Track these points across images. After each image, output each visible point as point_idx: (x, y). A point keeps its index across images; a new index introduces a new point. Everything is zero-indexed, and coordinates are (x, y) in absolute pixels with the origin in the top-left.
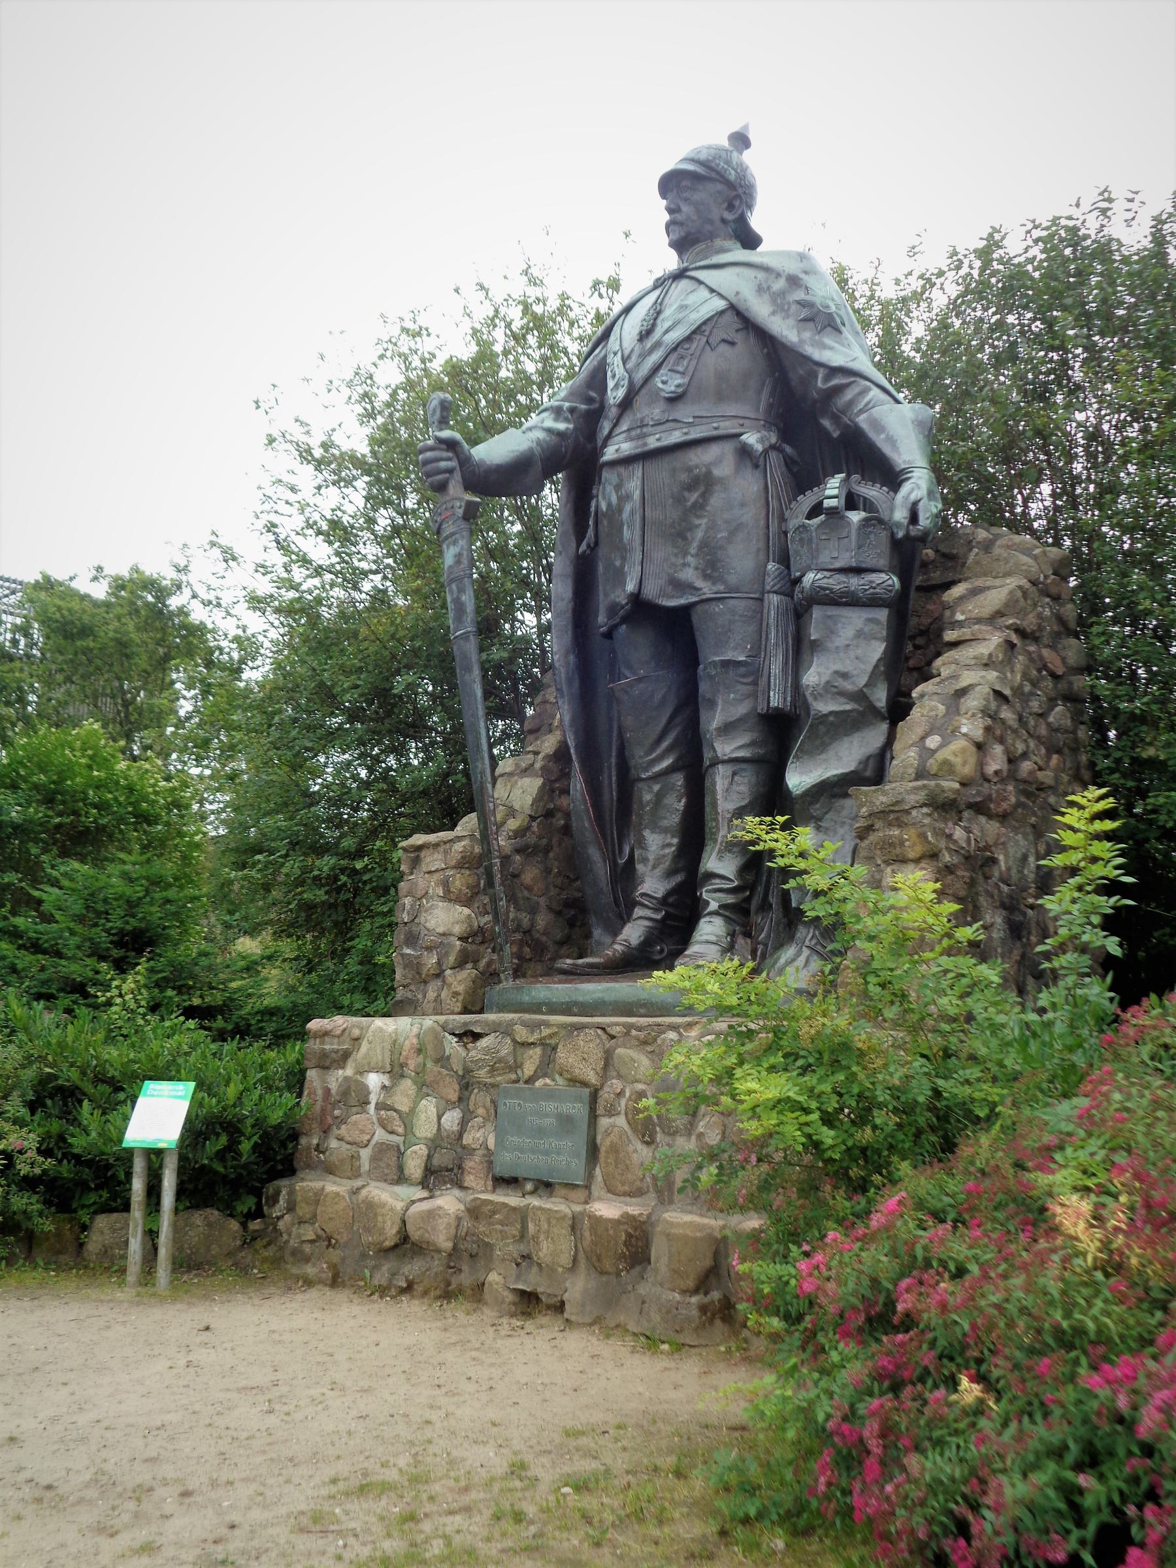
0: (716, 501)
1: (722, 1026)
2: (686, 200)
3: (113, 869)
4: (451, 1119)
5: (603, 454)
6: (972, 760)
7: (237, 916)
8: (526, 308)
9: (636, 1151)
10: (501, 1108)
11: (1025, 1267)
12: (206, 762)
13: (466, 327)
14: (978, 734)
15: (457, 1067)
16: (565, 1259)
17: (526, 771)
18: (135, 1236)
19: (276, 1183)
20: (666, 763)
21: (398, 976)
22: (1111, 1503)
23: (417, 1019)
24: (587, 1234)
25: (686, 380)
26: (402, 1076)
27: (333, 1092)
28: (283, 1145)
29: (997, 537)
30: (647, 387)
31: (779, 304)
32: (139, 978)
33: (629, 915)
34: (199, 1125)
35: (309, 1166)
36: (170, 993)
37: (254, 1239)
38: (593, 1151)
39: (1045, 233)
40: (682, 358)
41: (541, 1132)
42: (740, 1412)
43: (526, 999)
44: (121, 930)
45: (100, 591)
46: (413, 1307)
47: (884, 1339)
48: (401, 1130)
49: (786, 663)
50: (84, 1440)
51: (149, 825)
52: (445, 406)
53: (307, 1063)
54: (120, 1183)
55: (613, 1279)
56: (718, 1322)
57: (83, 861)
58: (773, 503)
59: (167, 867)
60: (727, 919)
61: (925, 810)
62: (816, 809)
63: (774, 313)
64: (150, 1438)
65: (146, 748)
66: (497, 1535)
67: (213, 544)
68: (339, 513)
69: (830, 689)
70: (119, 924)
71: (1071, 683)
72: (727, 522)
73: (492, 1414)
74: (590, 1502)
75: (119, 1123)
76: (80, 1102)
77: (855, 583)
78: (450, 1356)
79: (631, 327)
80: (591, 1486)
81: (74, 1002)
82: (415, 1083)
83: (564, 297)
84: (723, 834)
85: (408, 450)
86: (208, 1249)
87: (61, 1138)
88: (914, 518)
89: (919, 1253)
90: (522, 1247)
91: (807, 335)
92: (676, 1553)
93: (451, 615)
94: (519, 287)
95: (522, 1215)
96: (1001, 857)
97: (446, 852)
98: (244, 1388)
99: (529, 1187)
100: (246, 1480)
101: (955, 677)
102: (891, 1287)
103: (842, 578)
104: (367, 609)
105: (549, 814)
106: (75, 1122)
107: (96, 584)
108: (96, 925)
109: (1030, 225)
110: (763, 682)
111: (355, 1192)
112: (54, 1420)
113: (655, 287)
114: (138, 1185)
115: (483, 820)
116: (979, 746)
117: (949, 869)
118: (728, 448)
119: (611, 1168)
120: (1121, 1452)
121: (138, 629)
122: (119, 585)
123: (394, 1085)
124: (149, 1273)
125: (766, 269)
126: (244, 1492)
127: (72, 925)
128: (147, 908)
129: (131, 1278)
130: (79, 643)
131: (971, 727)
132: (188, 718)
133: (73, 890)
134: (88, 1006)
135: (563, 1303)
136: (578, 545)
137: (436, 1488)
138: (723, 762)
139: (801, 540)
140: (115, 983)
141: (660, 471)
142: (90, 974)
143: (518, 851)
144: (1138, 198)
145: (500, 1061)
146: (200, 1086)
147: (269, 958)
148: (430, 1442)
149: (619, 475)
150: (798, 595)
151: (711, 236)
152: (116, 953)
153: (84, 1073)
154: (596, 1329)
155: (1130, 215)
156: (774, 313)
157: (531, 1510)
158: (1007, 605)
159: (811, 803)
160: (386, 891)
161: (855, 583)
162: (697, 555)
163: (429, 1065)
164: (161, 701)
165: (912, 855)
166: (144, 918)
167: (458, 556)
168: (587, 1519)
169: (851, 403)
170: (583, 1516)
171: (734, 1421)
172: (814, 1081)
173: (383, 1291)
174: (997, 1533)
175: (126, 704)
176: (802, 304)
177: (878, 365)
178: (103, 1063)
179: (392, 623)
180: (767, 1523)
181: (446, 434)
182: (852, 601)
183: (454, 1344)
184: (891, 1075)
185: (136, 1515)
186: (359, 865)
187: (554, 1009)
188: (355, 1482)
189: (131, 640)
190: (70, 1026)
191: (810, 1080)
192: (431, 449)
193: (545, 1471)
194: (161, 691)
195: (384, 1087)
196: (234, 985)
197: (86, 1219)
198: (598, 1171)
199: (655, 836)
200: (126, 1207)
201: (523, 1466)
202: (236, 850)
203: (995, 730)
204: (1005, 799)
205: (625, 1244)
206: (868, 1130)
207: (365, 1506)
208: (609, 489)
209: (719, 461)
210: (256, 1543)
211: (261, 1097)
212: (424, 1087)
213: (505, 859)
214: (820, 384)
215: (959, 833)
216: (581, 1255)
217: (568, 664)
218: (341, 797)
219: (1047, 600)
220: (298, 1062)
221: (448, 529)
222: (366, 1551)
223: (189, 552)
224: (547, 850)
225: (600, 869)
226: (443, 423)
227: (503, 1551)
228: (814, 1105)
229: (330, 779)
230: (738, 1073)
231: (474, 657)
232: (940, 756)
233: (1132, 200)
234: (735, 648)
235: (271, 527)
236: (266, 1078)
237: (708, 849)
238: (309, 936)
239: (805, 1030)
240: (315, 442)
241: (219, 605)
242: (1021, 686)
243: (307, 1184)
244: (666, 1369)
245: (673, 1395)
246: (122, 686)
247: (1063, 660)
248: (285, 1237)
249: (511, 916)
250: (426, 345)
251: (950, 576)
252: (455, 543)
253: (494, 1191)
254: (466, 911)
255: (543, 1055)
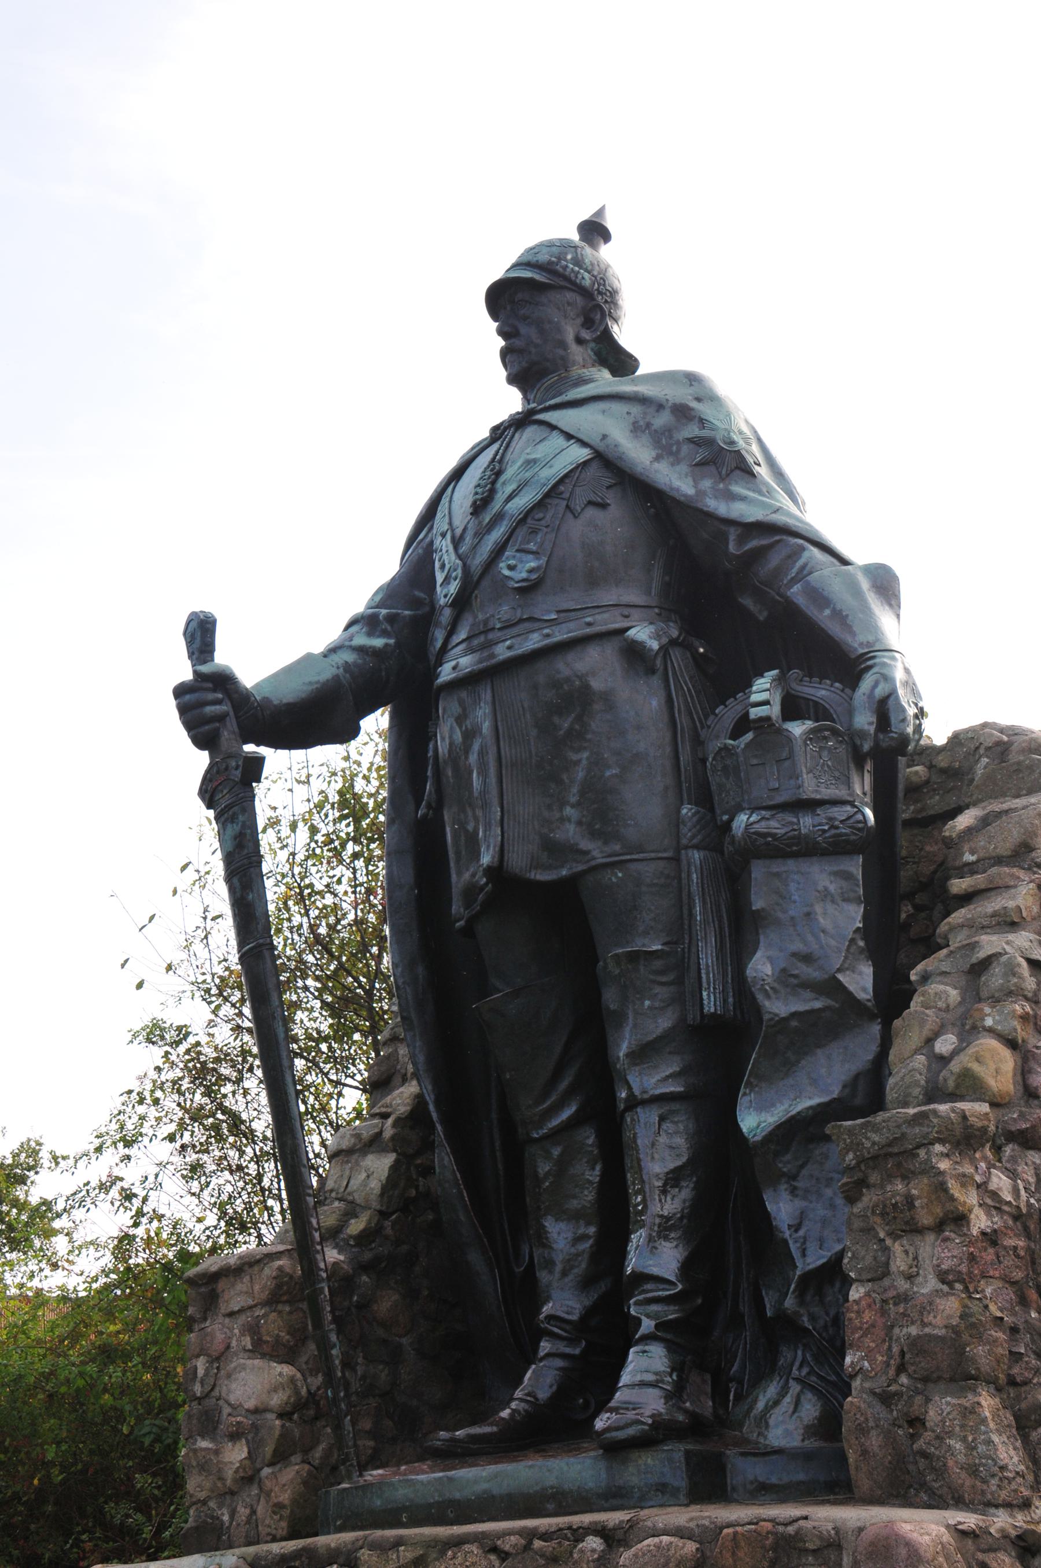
2: (525, 318)
5: (438, 676)
20: (566, 1114)
25: (543, 561)
60: (671, 1347)
62: (786, 1163)
63: (658, 458)
91: (706, 484)
125: (642, 400)
139: (725, 768)
143: (365, 1267)
149: (461, 703)
150: (728, 848)
156: (658, 458)
176: (696, 442)
199: (562, 1225)
214: (732, 548)
232: (955, 1066)
234: (646, 933)
251: (953, 801)
254: (287, 1370)
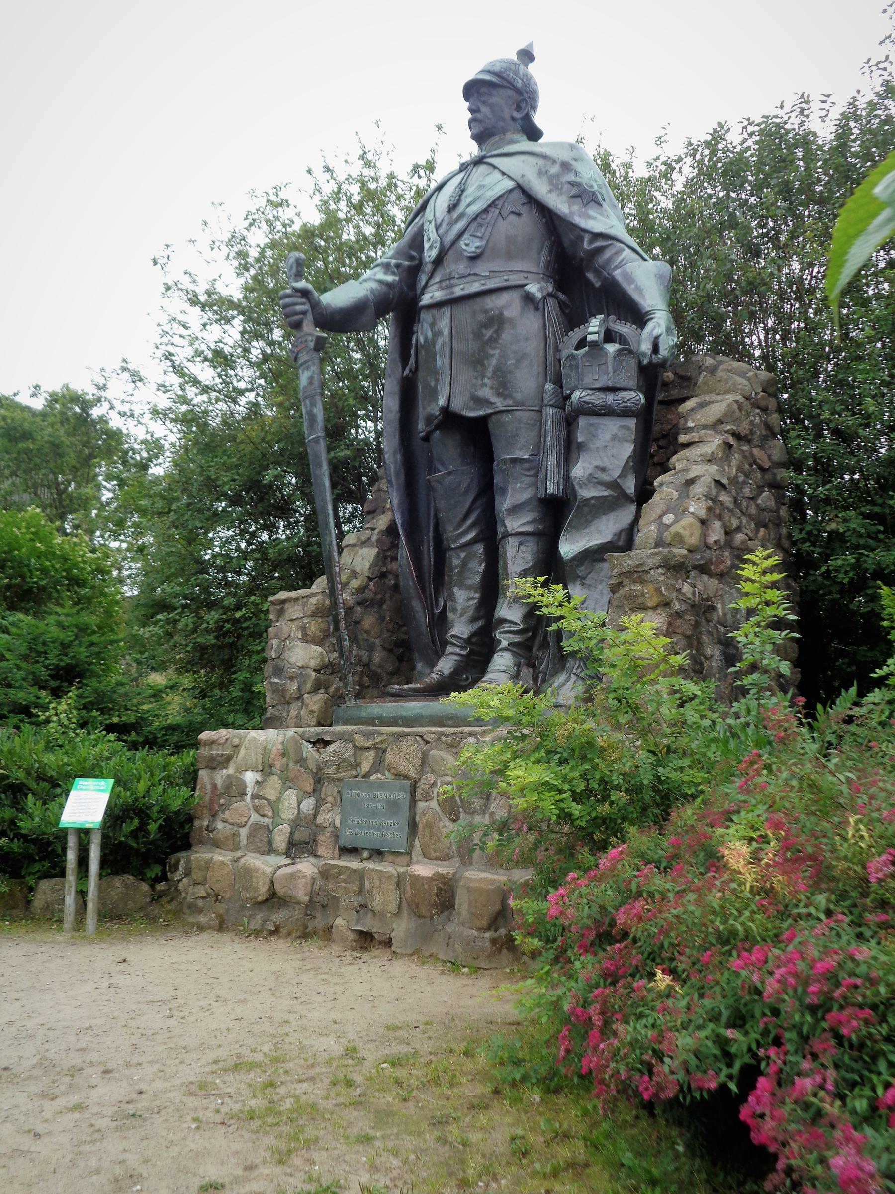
0: (506, 336)
1: (503, 731)
2: (484, 103)
3: (52, 619)
4: (308, 805)
6: (697, 533)
7: (146, 655)
8: (364, 185)
9: (445, 826)
10: (345, 796)
11: (697, 890)
12: (122, 537)
13: (317, 198)
14: (702, 513)
15: (312, 766)
16: (392, 908)
17: (365, 543)
18: (69, 894)
19: (178, 854)
21: (268, 699)
22: (750, 1050)
23: (282, 731)
24: (408, 888)
25: (484, 243)
26: (271, 774)
27: (219, 786)
28: (182, 826)
29: (720, 363)
30: (454, 248)
31: (555, 184)
32: (70, 701)
33: (443, 651)
34: (117, 811)
35: (201, 842)
36: (95, 713)
37: (160, 897)
38: (413, 826)
39: (757, 129)
40: (481, 226)
41: (374, 813)
42: (511, 1011)
43: (364, 714)
44: (57, 666)
45: (38, 404)
46: (279, 944)
47: (608, 948)
48: (270, 814)
49: (559, 460)
50: (30, 1037)
51: (79, 586)
52: (299, 263)
53: (200, 765)
54: (58, 856)
55: (428, 920)
56: (505, 951)
57: (27, 613)
58: (550, 338)
59: (92, 620)
60: (515, 654)
61: (660, 570)
62: (581, 571)
63: (550, 191)
64: (81, 1035)
65: (76, 527)
66: (333, 1095)
67: (124, 369)
68: (221, 345)
69: (592, 480)
70: (55, 661)
71: (775, 474)
72: (515, 352)
73: (333, 1016)
74: (402, 1073)
75: (56, 810)
76: (26, 795)
77: (611, 399)
78: (305, 978)
79: (442, 202)
80: (403, 1062)
81: (21, 721)
82: (281, 778)
83: (391, 176)
84: (511, 592)
85: (273, 296)
86: (126, 905)
87: (13, 822)
88: (656, 349)
89: (634, 889)
90: (360, 899)
91: (575, 208)
92: (462, 1105)
93: (305, 424)
94: (357, 167)
95: (360, 875)
96: (719, 606)
97: (304, 605)
98: (152, 1002)
99: (366, 854)
100: (151, 1062)
101: (686, 470)
102: (613, 911)
103: (601, 395)
104: (244, 419)
105: (383, 576)
106: (22, 810)
107: (35, 398)
108: (37, 662)
109: (746, 123)
110: (542, 475)
111: (236, 860)
112: (10, 1024)
113: (461, 171)
114: (71, 856)
115: (331, 580)
116: (703, 522)
117: (679, 615)
118: (515, 295)
119: (427, 839)
120: (758, 1014)
121: (68, 434)
122: (54, 399)
123: (264, 780)
124: (81, 922)
125: (545, 157)
126: (150, 1070)
127: (18, 662)
128: (76, 649)
129: (67, 925)
130: (20, 445)
131: (697, 508)
132: (108, 504)
133: (19, 635)
134: (31, 723)
135: (391, 940)
136: (404, 369)
137: (290, 1065)
138: (512, 535)
139: (571, 366)
140: (52, 706)
141: (464, 313)
142: (33, 699)
144: (830, 100)
145: (344, 761)
146: (118, 782)
147: (171, 687)
148: (287, 1035)
151: (504, 131)
152: (53, 683)
153: (28, 773)
154: (415, 957)
155: (824, 113)
156: (550, 191)
157: (358, 1079)
158: (726, 415)
159: (577, 566)
160: (260, 635)
161: (611, 399)
162: (492, 377)
163: (291, 765)
164: (88, 490)
165: (650, 604)
166: (74, 657)
167: (311, 379)
168: (399, 1083)
169: (609, 261)
170: (396, 1082)
171: (512, 1019)
172: (568, 770)
173: (257, 933)
174: (672, 1072)
175: (60, 493)
176: (572, 184)
177: (631, 231)
178: (43, 766)
179: (262, 429)
180: (529, 1084)
181: (302, 284)
182: (608, 412)
183: (309, 970)
184: (624, 764)
185: (70, 1086)
186: (238, 615)
187: (384, 722)
188: (231, 1062)
189: (62, 442)
190: (17, 738)
191: (565, 769)
192: (289, 296)
193: (371, 1054)
194: (87, 482)
195: (257, 782)
196: (145, 707)
197: (32, 882)
198: (417, 842)
199: (462, 592)
200: (63, 874)
201: (355, 1050)
202: (145, 606)
203: (715, 510)
204: (722, 562)
205: (436, 895)
206: (607, 805)
207: (238, 1077)
208: (426, 327)
209: (508, 305)
210: (157, 1103)
211: (164, 790)
212: (288, 781)
213: (349, 610)
215: (686, 588)
216: (404, 904)
217: (395, 461)
218: (227, 564)
219: (758, 411)
220: (192, 764)
221: (303, 357)
222: (238, 1107)
223: (106, 374)
224: (381, 603)
225: (421, 617)
226: (299, 275)
227: (337, 1105)
228: (566, 787)
229: (217, 549)
230: (512, 765)
231: (324, 456)
232: (673, 530)
233: (825, 102)
234: (521, 449)
235: (168, 356)
236: (168, 776)
237: (500, 601)
238: (203, 672)
239: (560, 732)
240: (201, 290)
241: (132, 416)
242: (736, 477)
243: (200, 855)
244: (465, 985)
245: (470, 1002)
246: (56, 479)
247: (769, 456)
248: (184, 895)
249: (354, 653)
250: (286, 214)
251: (685, 393)
252: (308, 368)
253: (339, 858)
254: (319, 649)
255: (376, 757)
